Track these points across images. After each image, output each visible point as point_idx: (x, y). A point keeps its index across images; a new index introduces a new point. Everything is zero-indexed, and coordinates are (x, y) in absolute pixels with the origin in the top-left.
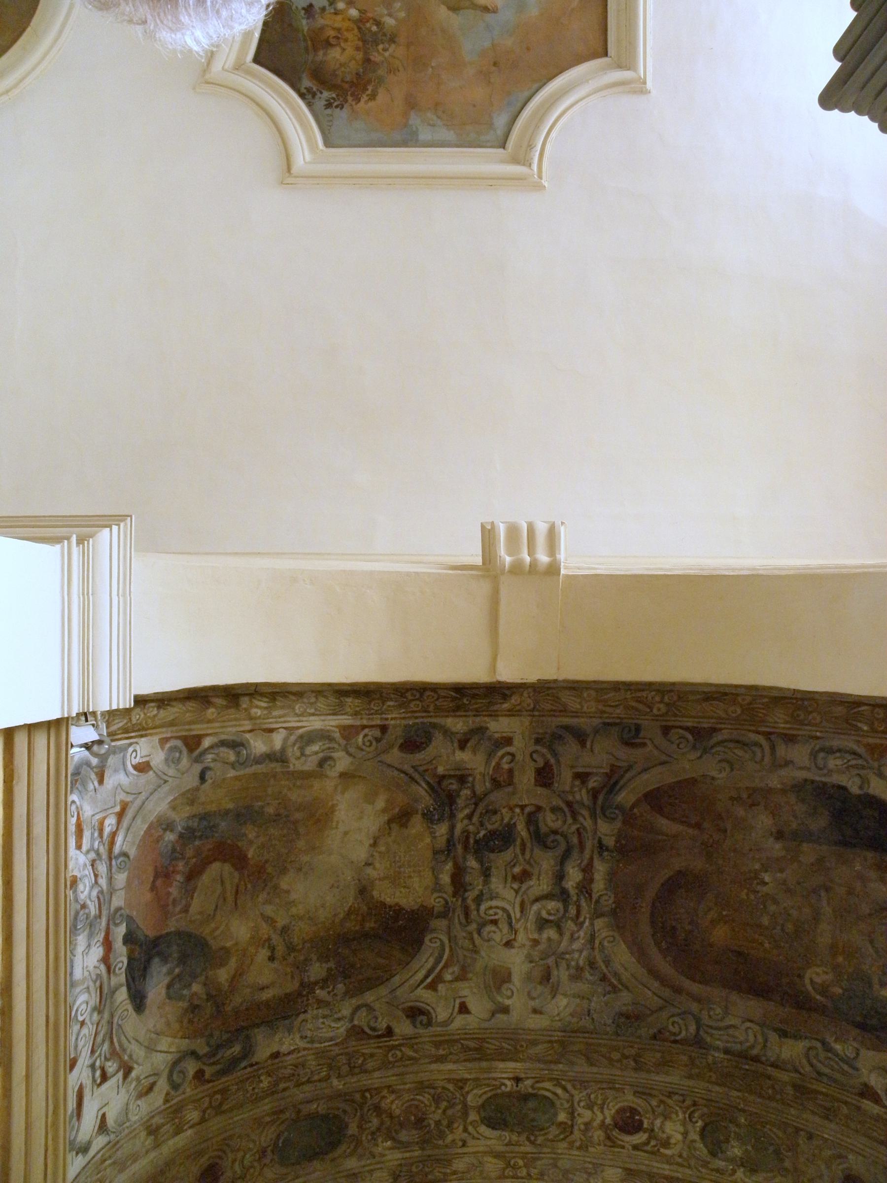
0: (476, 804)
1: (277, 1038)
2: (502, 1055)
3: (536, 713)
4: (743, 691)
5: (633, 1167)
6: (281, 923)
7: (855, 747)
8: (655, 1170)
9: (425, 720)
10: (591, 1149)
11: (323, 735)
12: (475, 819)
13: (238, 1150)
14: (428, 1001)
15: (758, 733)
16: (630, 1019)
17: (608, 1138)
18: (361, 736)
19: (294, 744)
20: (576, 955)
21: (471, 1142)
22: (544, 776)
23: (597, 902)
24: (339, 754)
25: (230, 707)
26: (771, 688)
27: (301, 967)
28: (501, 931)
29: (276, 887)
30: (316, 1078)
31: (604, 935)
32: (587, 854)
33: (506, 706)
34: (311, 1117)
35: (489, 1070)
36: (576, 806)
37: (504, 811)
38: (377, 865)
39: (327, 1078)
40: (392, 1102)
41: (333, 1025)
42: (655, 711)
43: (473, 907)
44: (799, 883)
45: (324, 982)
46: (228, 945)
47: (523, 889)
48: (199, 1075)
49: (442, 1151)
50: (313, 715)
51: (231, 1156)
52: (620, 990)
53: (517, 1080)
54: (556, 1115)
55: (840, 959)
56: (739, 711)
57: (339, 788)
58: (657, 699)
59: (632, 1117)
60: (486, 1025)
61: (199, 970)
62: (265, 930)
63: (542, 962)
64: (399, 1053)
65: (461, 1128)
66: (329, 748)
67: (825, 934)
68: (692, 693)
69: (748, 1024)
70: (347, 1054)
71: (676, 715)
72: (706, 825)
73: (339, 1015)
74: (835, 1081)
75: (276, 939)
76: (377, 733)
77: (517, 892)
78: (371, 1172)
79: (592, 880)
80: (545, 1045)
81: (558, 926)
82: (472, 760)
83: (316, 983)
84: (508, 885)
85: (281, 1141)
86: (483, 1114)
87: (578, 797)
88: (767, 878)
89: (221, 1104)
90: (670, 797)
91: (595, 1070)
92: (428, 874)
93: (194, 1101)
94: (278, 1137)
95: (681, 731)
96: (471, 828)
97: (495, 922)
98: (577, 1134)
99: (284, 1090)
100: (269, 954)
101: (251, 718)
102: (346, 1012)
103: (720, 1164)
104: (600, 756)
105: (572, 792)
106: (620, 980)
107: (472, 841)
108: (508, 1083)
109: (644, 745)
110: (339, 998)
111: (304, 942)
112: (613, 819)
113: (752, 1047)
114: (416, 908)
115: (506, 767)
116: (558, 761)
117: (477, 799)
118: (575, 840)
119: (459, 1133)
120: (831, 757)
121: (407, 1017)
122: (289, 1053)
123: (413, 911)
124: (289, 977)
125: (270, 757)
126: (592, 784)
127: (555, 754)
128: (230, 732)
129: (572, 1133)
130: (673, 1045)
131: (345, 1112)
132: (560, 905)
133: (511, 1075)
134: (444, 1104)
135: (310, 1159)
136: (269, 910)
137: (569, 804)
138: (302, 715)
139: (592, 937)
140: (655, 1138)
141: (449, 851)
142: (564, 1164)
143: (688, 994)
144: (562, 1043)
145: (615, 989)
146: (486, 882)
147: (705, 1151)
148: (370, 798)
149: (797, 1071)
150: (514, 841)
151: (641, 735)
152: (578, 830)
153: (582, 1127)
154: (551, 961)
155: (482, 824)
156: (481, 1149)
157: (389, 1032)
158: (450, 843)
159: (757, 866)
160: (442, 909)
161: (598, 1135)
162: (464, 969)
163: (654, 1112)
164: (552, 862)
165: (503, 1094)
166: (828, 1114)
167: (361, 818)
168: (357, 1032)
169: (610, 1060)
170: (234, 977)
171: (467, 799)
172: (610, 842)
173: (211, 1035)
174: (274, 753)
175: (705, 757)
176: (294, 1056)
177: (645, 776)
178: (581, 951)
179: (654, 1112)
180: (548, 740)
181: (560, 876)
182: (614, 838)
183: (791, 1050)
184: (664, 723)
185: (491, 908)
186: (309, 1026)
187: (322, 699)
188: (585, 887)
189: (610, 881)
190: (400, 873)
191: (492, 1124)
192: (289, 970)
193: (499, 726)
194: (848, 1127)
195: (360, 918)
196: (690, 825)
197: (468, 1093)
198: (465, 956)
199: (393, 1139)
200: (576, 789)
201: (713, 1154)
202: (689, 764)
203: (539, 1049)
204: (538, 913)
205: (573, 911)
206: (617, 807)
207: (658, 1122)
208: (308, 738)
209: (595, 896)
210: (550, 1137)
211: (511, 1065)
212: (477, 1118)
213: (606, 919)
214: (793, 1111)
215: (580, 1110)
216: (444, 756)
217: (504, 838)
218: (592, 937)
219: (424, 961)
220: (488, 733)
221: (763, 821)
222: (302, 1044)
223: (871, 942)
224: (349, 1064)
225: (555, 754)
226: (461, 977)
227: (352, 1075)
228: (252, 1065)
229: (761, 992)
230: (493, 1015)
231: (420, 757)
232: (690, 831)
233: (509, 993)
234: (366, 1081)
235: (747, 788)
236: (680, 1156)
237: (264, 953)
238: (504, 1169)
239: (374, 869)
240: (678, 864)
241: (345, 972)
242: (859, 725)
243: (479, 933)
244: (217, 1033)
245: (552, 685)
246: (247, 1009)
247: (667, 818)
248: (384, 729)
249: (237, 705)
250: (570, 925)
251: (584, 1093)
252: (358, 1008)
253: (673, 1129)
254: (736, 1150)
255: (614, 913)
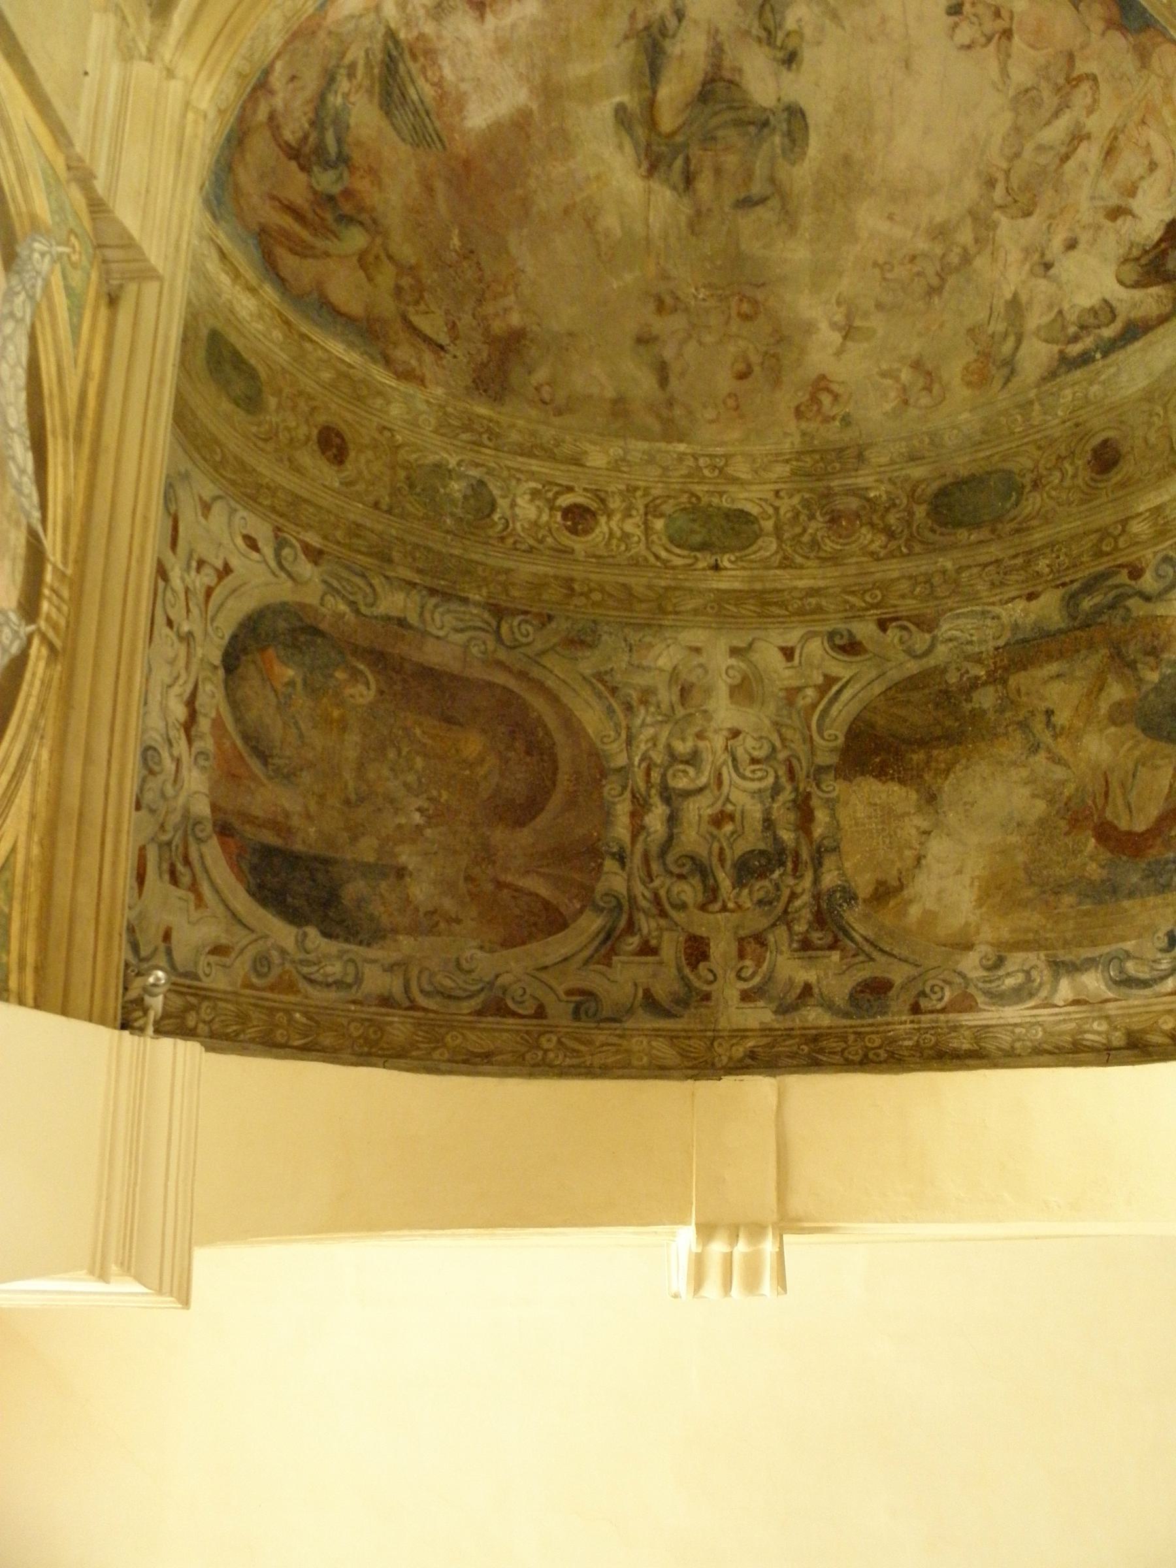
0: (786, 912)
1: (1033, 617)
2: (738, 597)
3: (710, 1034)
4: (443, 1066)
5: (573, 468)
6: (1041, 757)
7: (310, 989)
8: (547, 464)
9: (859, 1022)
10: (623, 487)
11: (999, 998)
12: (786, 893)
13: (1070, 489)
14: (834, 662)
15: (425, 1010)
16: (579, 641)
17: (603, 501)
18: (946, 999)
19: (1041, 985)
20: (649, 720)
21: (770, 496)
22: (697, 950)
23: (624, 788)
24: (977, 974)
25: (1139, 1031)
26: (408, 1070)
27: (1008, 703)
28: (746, 750)
29: (1051, 802)
30: (975, 570)
31: (615, 746)
32: (639, 847)
33: (751, 1043)
34: (977, 525)
35: (752, 579)
36: (654, 911)
37: (748, 904)
38: (913, 831)
39: (959, 570)
40: (872, 541)
41: (958, 633)
42: (554, 1039)
43: (783, 780)
44: (379, 810)
45: (975, 684)
46: (1113, 729)
47: (720, 803)
48: (1136, 573)
49: (804, 485)
50: (1016, 1025)
51: (1080, 481)
52: (594, 676)
53: (716, 567)
54: (667, 526)
55: (336, 714)
56: (448, 1039)
57: (972, 929)
58: (551, 1055)
59: (575, 524)
60: (758, 633)
61: (1152, 697)
62: (1062, 748)
63: (692, 710)
64: (868, 598)
65: (782, 511)
66: (990, 982)
67: (351, 746)
68: (506, 1064)
69: (441, 633)
70: (936, 598)
71: (527, 1032)
72: (489, 887)
73: (951, 645)
74: (348, 568)
75: (1047, 738)
76: (924, 1003)
77: (728, 800)
78: (892, 462)
79: (633, 815)
80: (683, 608)
81: (673, 757)
82: (793, 970)
83: (984, 684)
84: (739, 808)
85: (1014, 498)
86: (756, 526)
87: (653, 924)
88: (417, 818)
89: (1101, 540)
90: (535, 924)
91: (622, 580)
92: (845, 822)
93: (1138, 543)
94: (1017, 504)
95: (521, 1011)
96: (791, 881)
97: (754, 761)
98: (640, 504)
99: (1015, 556)
100: (1053, 719)
101: (1107, 1017)
102: (942, 649)
103: (474, 472)
104: (624, 978)
105: (660, 929)
106: (594, 688)
107: (790, 865)
108: (726, 564)
109: (569, 993)
110: (953, 666)
111: (1006, 734)
112: (607, 894)
113: (436, 606)
114: (859, 779)
115: (748, 962)
116: (680, 970)
117: (786, 918)
118: (655, 867)
119: (786, 505)
120: (338, 977)
121: (860, 643)
122: (1013, 599)
123: (863, 774)
124: (1023, 690)
125: (1074, 968)
126: (634, 942)
127: (683, 978)
128: (1137, 999)
129: (646, 506)
130: (526, 608)
131: (933, 531)
132: (672, 783)
133: (724, 573)
134: (806, 539)
135: (973, 477)
136: (1059, 773)
137: (663, 914)
138: (1033, 1024)
139: (629, 741)
140: (548, 500)
141: (818, 851)
142: (654, 471)
143: (510, 671)
144: (662, 610)
145: (599, 676)
146: (767, 813)
147: (491, 486)
148: (929, 918)
149: (387, 578)
150: (734, 865)
151: (572, 1005)
152: (652, 881)
153: (634, 513)
154: (680, 712)
155: (777, 887)
156: (754, 488)
157: (883, 625)
158: (818, 864)
159: (428, 832)
160: (823, 776)
161: (615, 503)
162: (790, 703)
163: (550, 531)
164: (683, 838)
165: (731, 550)
166: (356, 530)
167: (939, 893)
168: (926, 624)
169: (602, 590)
170: (1101, 689)
171: (798, 920)
172: (610, 864)
173: (1124, 620)
174: (1068, 972)
175: (492, 976)
176: (1006, 597)
177: (565, 951)
178: (643, 724)
179: (550, 531)
180: (693, 998)
181: (672, 820)
182: (606, 869)
183: (393, 602)
184: (544, 1022)
185: (760, 779)
186: (990, 632)
187: (1006, 1046)
188: (640, 807)
189: (608, 814)
190: (883, 822)
191: (743, 516)
192: (1024, 699)
193: (759, 1015)
194: (336, 516)
195: (933, 765)
196: (508, 886)
197: (777, 552)
198: (790, 718)
199: (868, 500)
200: (655, 934)
201: (481, 483)
202: (512, 967)
203: (691, 604)
204: (699, 771)
205: (655, 776)
206: (601, 910)
207: (545, 518)
208: (1020, 994)
209: (628, 794)
210: (672, 501)
211: (723, 586)
212: (762, 523)
213: (612, 765)
214: (394, 532)
215: (638, 532)
216: (831, 975)
217: (748, 869)
218: (629, 741)
219: (843, 711)
220: (774, 1006)
221: (421, 891)
222: (997, 610)
223: (301, 736)
224: (932, 586)
225: (683, 978)
226: (793, 693)
227: (926, 574)
228: (1064, 585)
229: (427, 673)
230: (750, 645)
231: (864, 973)
232: (509, 878)
233: (731, 672)
234: (911, 566)
235: (440, 935)
236: (519, 480)
237: (1062, 718)
238: (726, 465)
239: (918, 828)
240: (524, 836)
241: (947, 698)
242: (304, 1020)
243: (774, 749)
244: (1117, 622)
245: (690, 1072)
246: (1078, 651)
247: (537, 895)
248: (916, 1009)
249: (1129, 1034)
250: (658, 757)
251: (633, 552)
252: (926, 653)
253: (527, 510)
254: (456, 487)
255: (604, 774)
